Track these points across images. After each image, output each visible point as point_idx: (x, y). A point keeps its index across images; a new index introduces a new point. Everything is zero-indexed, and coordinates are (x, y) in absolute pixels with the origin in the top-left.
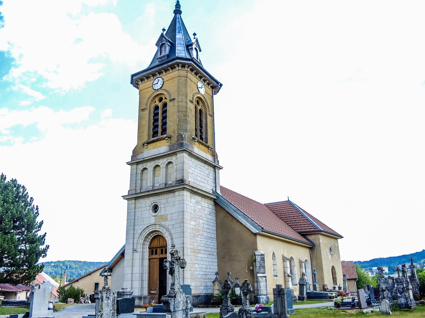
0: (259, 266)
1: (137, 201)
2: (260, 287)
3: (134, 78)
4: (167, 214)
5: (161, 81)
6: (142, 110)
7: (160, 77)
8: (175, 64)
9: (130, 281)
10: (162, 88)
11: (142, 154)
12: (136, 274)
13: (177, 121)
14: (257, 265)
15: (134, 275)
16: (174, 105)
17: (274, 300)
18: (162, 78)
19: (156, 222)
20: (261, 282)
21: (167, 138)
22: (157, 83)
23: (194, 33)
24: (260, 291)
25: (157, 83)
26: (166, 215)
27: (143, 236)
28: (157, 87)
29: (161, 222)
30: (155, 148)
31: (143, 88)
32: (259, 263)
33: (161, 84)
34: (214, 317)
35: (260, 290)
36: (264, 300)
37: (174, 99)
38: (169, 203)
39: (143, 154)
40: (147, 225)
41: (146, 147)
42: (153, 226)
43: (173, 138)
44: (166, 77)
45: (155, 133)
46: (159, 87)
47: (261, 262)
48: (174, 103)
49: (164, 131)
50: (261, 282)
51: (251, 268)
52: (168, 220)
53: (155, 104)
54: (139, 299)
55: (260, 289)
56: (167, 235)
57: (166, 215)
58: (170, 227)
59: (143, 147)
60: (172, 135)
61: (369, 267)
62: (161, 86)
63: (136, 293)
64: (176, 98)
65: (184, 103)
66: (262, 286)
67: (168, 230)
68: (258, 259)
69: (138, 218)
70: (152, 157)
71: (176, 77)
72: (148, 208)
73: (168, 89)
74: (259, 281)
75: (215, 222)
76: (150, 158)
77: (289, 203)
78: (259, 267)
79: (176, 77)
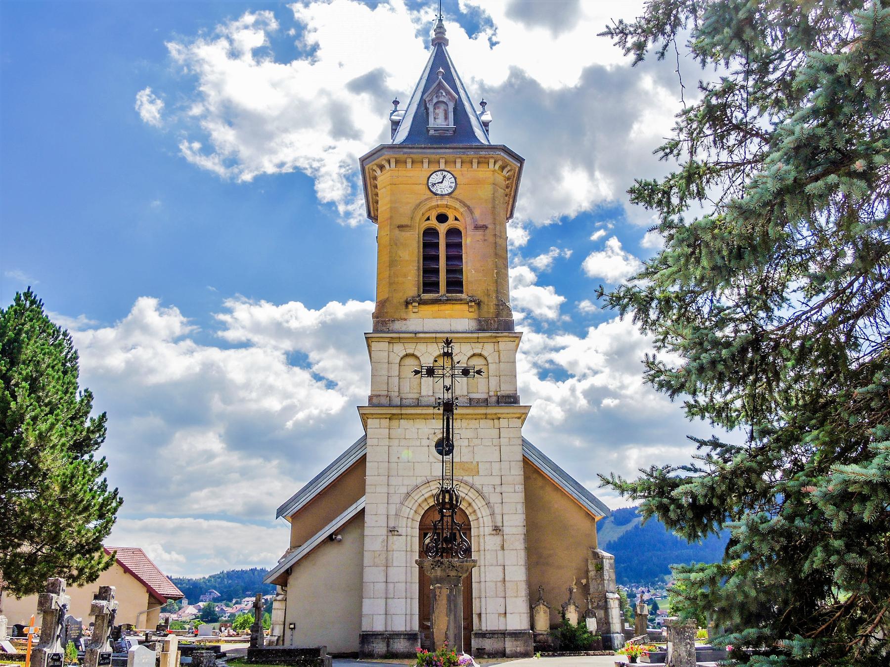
1: (395, 423)
6: (398, 227)
9: (381, 598)
10: (453, 195)
11: (404, 322)
12: (397, 585)
13: (493, 274)
15: (391, 586)
16: (485, 240)
17: (375, 635)
21: (473, 304)
22: (441, 181)
25: (442, 182)
26: (474, 463)
27: (429, 489)
33: (451, 187)
34: (82, 666)
36: (619, 643)
39: (408, 322)
41: (416, 310)
43: (486, 307)
45: (430, 285)
46: (447, 192)
49: (455, 285)
51: (584, 581)
52: (481, 473)
53: (428, 222)
54: (409, 639)
56: (480, 506)
58: (486, 490)
59: (404, 307)
60: (482, 299)
62: (450, 191)
63: (399, 625)
64: (489, 226)
67: (480, 493)
69: (397, 461)
72: (425, 442)
75: (523, 486)
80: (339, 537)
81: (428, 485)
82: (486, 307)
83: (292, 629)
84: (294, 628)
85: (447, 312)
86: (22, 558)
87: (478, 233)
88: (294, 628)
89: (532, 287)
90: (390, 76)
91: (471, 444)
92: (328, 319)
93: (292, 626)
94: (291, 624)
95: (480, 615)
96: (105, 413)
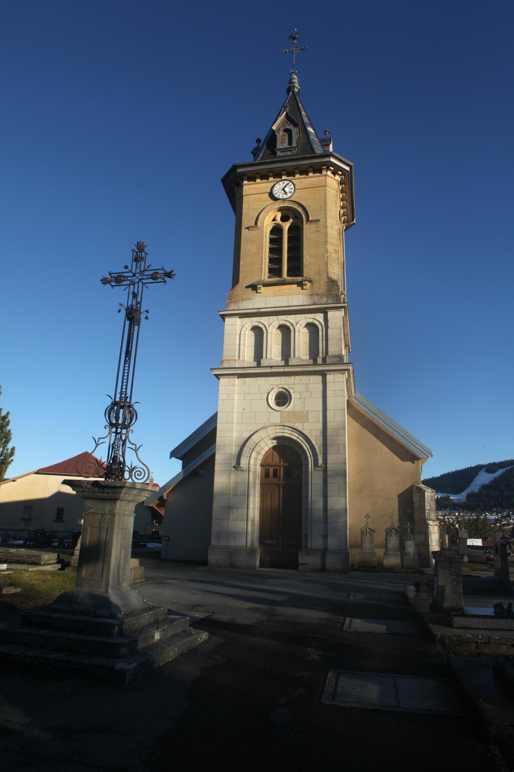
0: (429, 508)
2: (432, 541)
3: (239, 170)
4: (307, 412)
5: (291, 187)
7: (289, 181)
8: (324, 164)
14: (426, 506)
16: (318, 231)
18: (292, 182)
19: (282, 422)
20: (432, 533)
23: (257, 138)
24: (432, 547)
27: (282, 431)
28: (278, 193)
29: (295, 423)
30: (280, 295)
31: (251, 192)
32: (429, 504)
33: (290, 192)
35: (432, 545)
37: (318, 221)
38: (311, 392)
40: (264, 425)
42: (277, 427)
44: (301, 182)
47: (431, 502)
48: (317, 227)
50: (432, 533)
51: (409, 511)
52: (310, 420)
55: (432, 543)
57: (305, 412)
61: (392, 533)
65: (335, 231)
66: (433, 540)
68: (427, 499)
70: (277, 309)
71: (321, 187)
73: (304, 204)
74: (430, 531)
76: (273, 309)
77: (171, 452)
78: (429, 510)
79: (321, 187)
80: (202, 472)
81: (282, 427)
82: (317, 285)
83: (167, 540)
84: (169, 540)
85: (285, 291)
86: (43, 571)
87: (312, 226)
88: (169, 540)
89: (33, 474)
90: (121, 311)
91: (303, 397)
92: (281, 225)
93: (167, 538)
94: (166, 537)
95: (306, 536)
96: (105, 281)
